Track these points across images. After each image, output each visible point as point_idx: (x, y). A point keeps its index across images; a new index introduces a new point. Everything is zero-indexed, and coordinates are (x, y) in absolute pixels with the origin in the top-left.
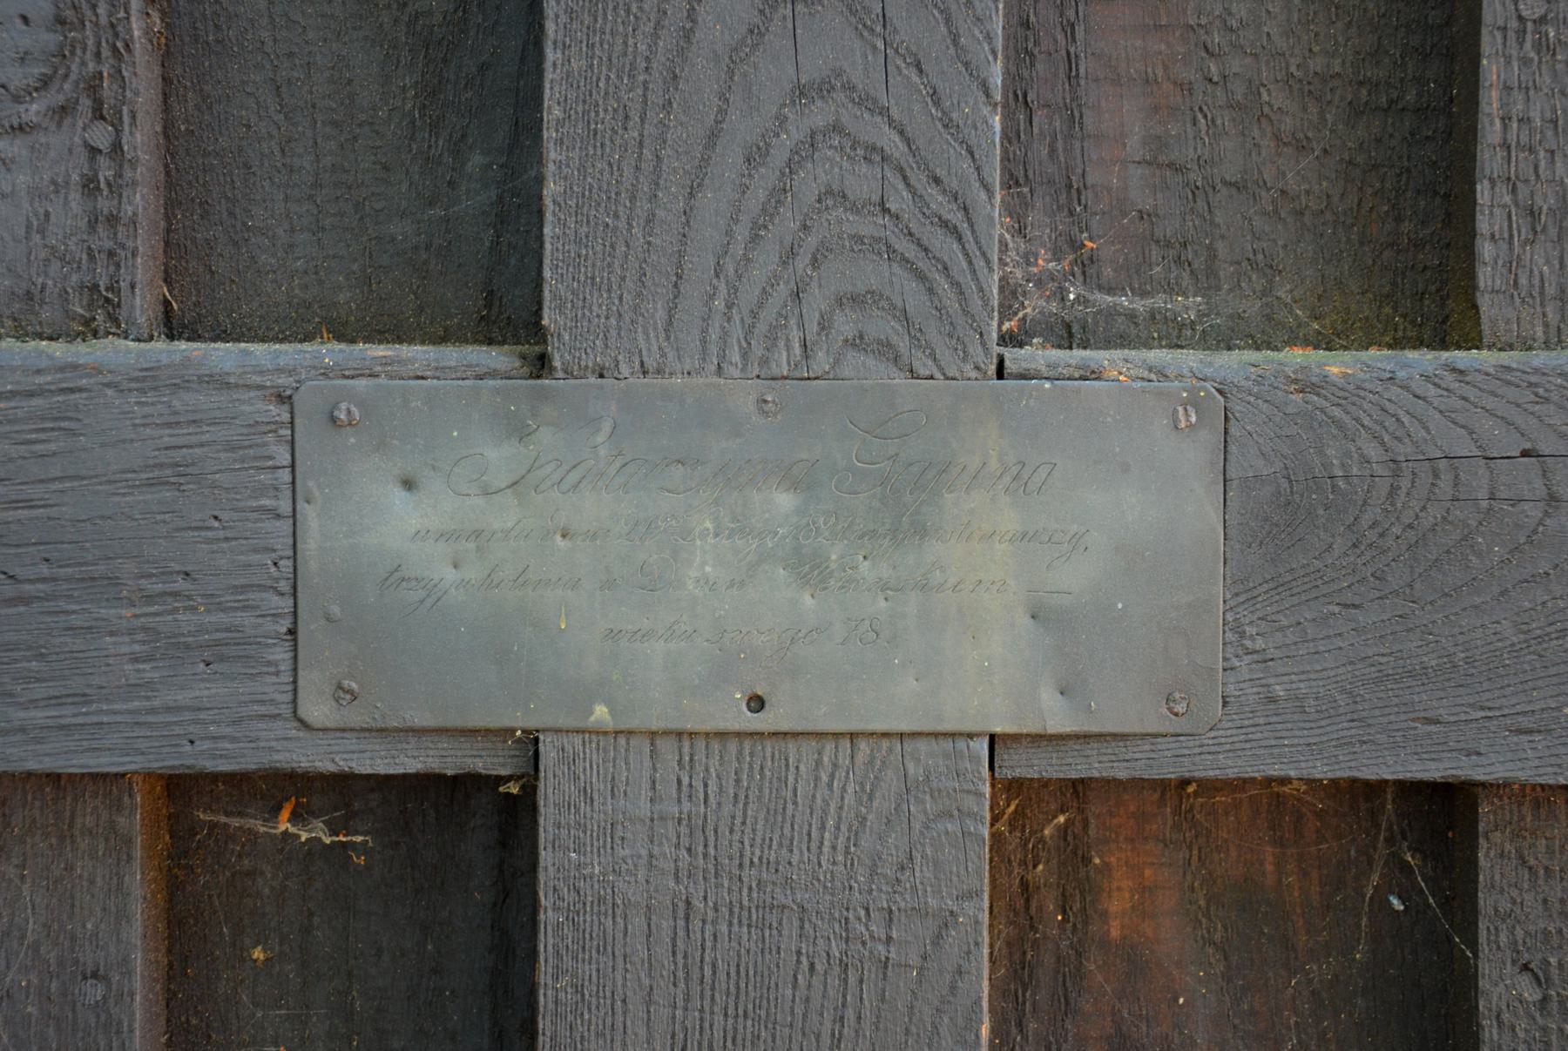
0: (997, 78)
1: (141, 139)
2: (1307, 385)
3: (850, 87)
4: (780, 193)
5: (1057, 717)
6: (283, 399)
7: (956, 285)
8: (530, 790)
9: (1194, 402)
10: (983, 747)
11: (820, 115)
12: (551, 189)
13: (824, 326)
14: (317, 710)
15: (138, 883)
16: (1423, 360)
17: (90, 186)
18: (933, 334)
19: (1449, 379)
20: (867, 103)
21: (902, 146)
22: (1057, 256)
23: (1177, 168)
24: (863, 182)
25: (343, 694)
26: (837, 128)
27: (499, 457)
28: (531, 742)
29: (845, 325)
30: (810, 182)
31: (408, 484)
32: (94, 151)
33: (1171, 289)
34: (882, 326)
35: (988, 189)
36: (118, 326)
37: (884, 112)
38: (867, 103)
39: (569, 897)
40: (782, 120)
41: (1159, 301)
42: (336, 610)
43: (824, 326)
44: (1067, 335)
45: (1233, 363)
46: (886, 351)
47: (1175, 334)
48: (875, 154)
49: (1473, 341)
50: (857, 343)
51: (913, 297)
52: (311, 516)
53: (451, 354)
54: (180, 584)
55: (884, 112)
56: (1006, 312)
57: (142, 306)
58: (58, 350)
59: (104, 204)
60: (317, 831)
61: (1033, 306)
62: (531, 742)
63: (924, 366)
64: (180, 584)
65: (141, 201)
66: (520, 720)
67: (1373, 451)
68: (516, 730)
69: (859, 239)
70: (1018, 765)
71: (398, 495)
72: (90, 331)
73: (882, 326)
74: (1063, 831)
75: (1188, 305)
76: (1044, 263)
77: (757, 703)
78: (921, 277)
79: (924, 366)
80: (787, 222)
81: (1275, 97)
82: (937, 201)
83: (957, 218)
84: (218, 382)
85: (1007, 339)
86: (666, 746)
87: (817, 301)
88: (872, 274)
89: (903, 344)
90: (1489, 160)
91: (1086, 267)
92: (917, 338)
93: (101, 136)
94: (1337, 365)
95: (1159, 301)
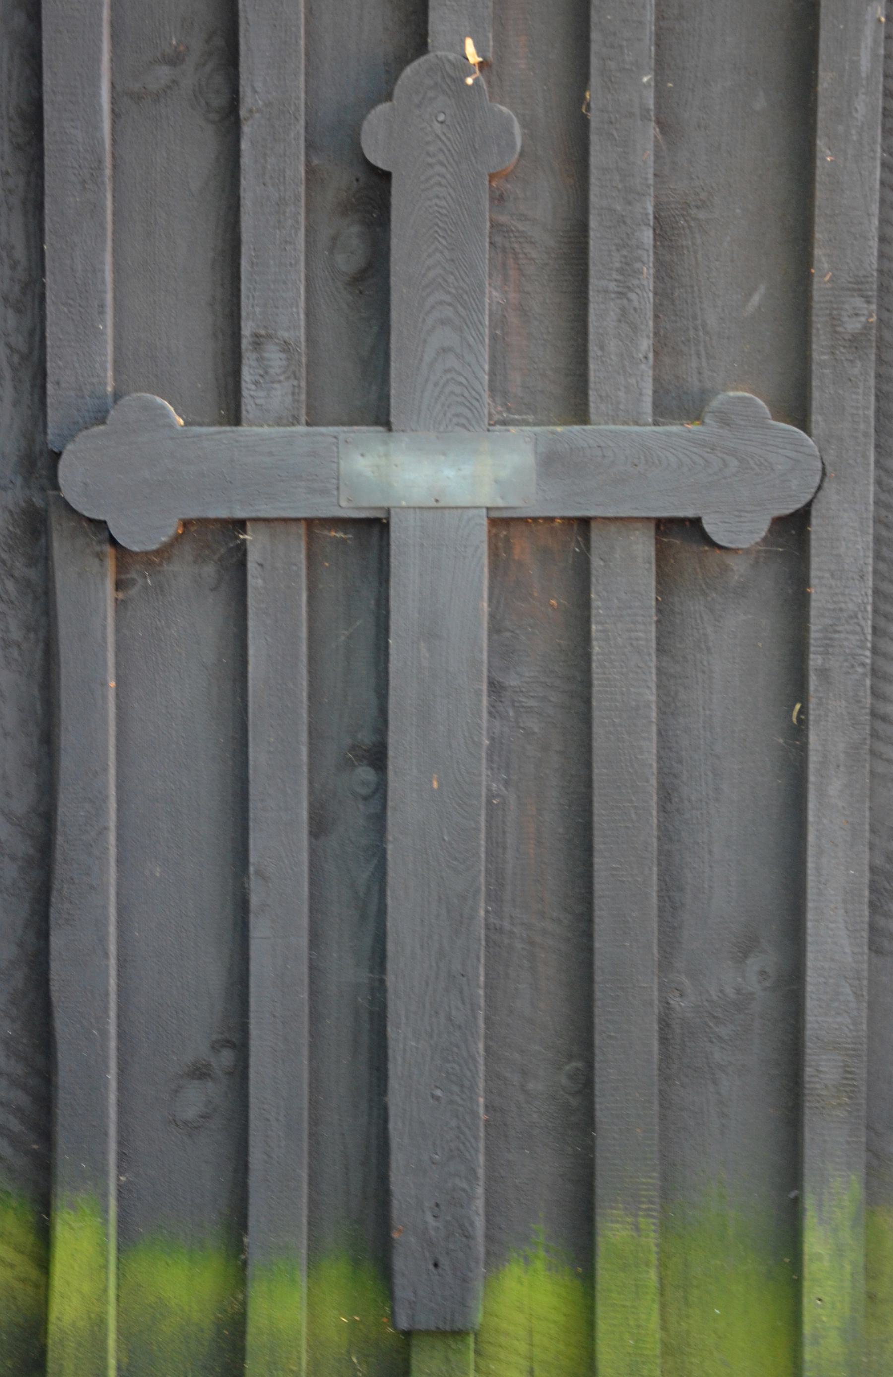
0: (487, 367)
1: (303, 384)
2: (553, 433)
3: (456, 371)
4: (441, 393)
5: (500, 503)
6: (336, 437)
7: (478, 411)
8: (388, 519)
9: (529, 437)
10: (484, 511)
11: (449, 376)
12: (393, 392)
13: (451, 420)
14: (344, 504)
15: (303, 545)
16: (577, 428)
17: (293, 394)
18: (474, 423)
19: (582, 431)
20: (460, 374)
21: (466, 381)
22: (502, 407)
23: (528, 388)
24: (458, 390)
25: (349, 500)
26: (453, 379)
27: (381, 449)
28: (388, 511)
29: (455, 420)
30: (447, 390)
31: (362, 455)
32: (294, 386)
33: (526, 414)
34: (463, 421)
35: (484, 391)
36: (299, 423)
37: (463, 376)
38: (460, 374)
39: (397, 542)
40: (441, 377)
41: (524, 417)
42: (347, 483)
43: (451, 420)
44: (504, 423)
45: (537, 429)
46: (464, 426)
47: (527, 423)
48: (461, 384)
49: (590, 424)
50: (458, 424)
51: (470, 415)
52: (342, 463)
53: (372, 428)
54: (315, 477)
55: (463, 376)
56: (490, 419)
57: (303, 419)
58: (289, 429)
59: (296, 398)
60: (340, 535)
61: (496, 417)
62: (388, 511)
63: (471, 428)
64: (315, 477)
65: (303, 397)
66: (385, 504)
67: (566, 446)
68: (244, 1254)
69: (457, 402)
70: (495, 514)
71: (360, 459)
72: (293, 424)
73: (463, 421)
74: (505, 536)
75: (531, 418)
76: (500, 408)
77: (437, 501)
78: (470, 409)
79: (471, 428)
80: (443, 398)
81: (549, 372)
82: (474, 393)
83: (478, 397)
84: (322, 434)
85: (490, 425)
86: (417, 511)
87: (449, 415)
88: (460, 409)
89: (467, 425)
90: (592, 385)
91: (508, 410)
92: (471, 424)
93: (295, 383)
94: (559, 429)
95: (524, 417)
